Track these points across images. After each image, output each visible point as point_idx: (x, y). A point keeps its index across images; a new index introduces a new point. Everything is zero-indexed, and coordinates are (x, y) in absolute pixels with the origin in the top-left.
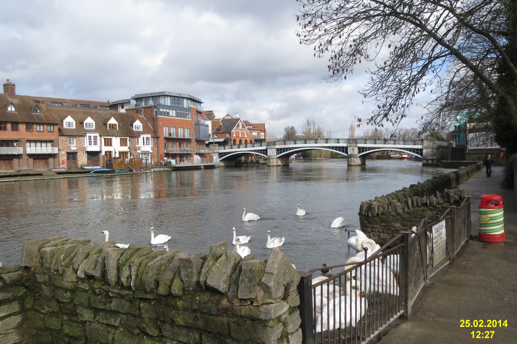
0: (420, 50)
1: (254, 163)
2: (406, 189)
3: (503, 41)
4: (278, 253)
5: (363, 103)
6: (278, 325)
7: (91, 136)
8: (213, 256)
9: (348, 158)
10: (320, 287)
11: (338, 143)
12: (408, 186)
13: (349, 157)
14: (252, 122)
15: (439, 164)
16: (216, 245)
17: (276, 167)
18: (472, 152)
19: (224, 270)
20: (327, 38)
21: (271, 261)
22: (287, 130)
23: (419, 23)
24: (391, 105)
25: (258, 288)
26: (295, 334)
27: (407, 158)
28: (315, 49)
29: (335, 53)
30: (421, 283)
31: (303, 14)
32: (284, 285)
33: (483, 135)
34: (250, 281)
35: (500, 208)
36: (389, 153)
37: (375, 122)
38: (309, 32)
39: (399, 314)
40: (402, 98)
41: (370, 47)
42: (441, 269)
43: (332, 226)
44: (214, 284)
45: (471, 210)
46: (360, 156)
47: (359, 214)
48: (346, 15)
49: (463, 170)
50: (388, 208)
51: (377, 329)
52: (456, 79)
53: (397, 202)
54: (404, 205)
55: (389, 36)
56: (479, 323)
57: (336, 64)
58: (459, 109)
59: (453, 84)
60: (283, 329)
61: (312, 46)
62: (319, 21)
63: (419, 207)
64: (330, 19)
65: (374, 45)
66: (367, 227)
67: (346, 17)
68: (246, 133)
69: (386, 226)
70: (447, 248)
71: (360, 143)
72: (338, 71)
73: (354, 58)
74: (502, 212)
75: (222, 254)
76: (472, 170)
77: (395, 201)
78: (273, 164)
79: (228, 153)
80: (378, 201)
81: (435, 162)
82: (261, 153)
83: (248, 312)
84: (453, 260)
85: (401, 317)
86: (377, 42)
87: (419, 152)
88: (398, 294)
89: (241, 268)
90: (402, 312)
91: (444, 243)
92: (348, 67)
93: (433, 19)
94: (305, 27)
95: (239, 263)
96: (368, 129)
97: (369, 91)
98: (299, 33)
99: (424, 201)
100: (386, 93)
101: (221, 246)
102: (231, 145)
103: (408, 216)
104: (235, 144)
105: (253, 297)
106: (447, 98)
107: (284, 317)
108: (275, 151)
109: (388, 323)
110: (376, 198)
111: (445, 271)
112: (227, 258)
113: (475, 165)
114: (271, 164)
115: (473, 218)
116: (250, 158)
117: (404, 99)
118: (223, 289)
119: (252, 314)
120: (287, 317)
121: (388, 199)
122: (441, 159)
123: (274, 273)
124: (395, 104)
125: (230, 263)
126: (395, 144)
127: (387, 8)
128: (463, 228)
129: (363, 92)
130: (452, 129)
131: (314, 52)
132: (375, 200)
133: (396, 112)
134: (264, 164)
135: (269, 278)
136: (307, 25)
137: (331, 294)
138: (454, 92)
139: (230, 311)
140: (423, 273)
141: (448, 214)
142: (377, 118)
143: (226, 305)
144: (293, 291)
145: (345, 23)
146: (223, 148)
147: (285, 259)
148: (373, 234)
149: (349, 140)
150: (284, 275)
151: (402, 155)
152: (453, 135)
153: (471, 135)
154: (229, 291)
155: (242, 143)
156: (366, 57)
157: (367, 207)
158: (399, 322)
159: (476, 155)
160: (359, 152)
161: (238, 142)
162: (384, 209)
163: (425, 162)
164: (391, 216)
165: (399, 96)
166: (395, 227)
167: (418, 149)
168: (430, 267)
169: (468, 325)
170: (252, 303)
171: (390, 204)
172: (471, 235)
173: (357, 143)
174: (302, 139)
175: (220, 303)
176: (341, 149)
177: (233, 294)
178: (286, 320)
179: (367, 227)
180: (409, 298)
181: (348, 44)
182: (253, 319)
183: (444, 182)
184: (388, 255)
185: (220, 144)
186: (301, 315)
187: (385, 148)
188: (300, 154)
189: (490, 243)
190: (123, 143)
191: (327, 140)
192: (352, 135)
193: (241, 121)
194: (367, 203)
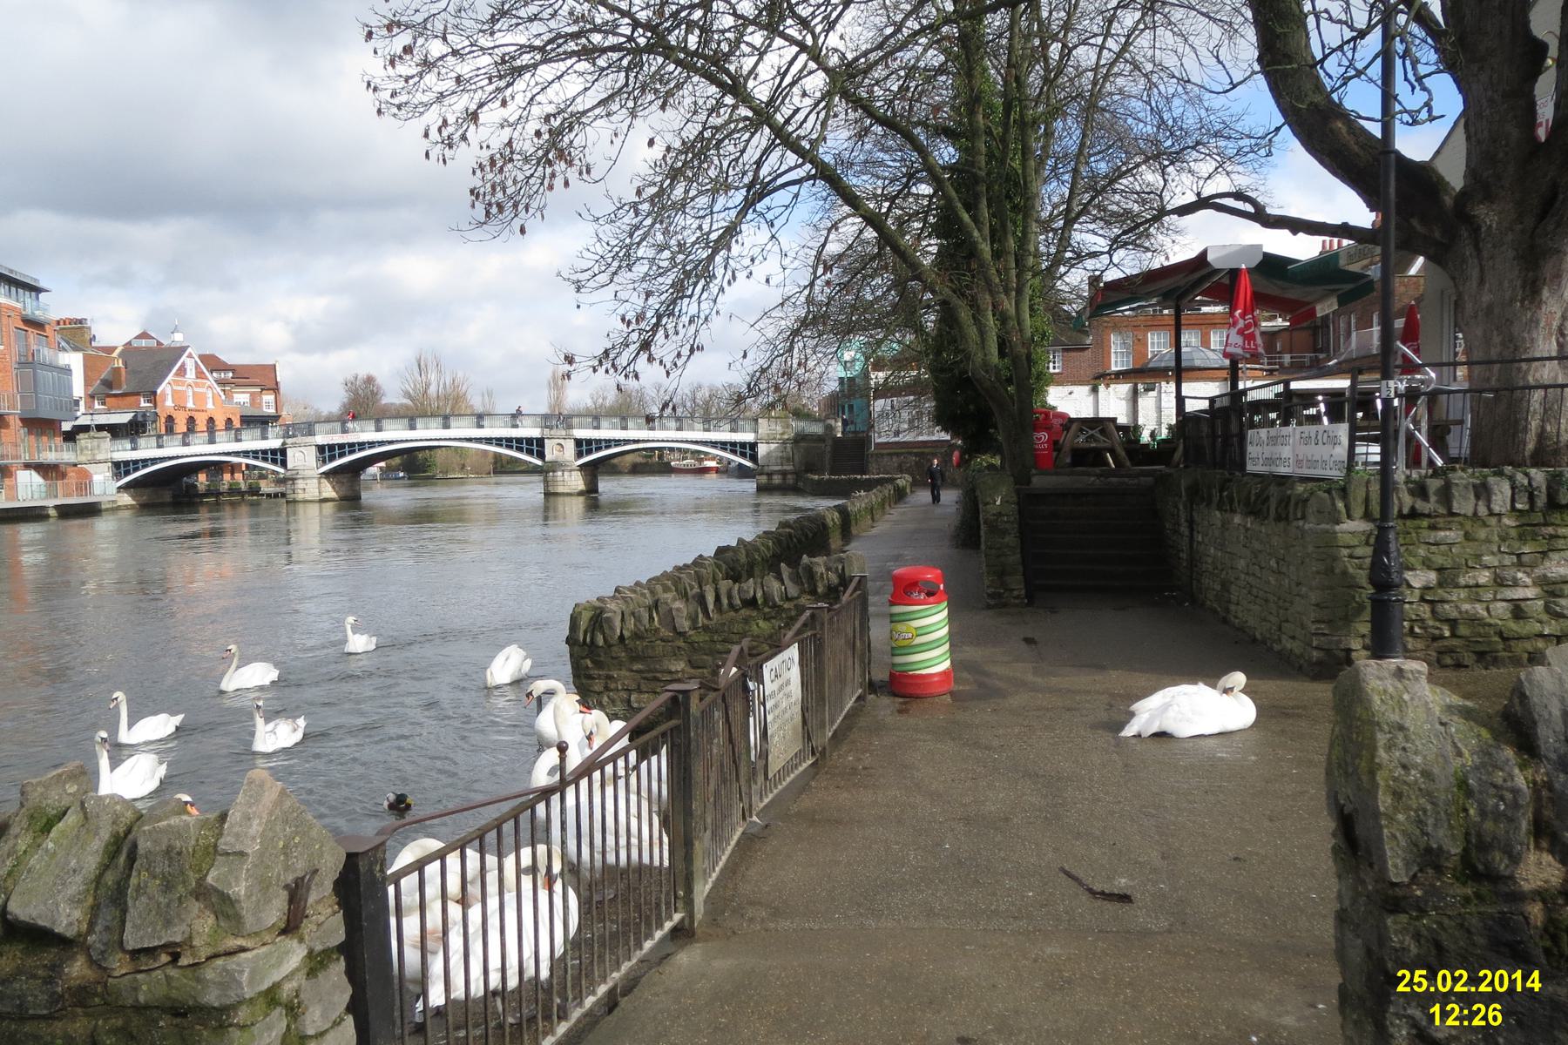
0: (737, 160)
1: (242, 494)
3: (946, 153)
4: (261, 786)
6: (267, 1015)
8: (32, 817)
9: (547, 472)
12: (710, 552)
15: (801, 484)
16: (43, 779)
17: (317, 505)
19: (73, 863)
20: (464, 102)
21: (238, 815)
22: (351, 386)
24: (659, 317)
25: (195, 906)
26: (329, 1037)
27: (717, 470)
28: (426, 135)
29: (491, 152)
30: (733, 829)
31: (386, 22)
32: (286, 887)
34: (168, 887)
35: (938, 602)
36: (667, 457)
37: (613, 365)
38: (406, 81)
39: (668, 925)
40: (690, 297)
41: (594, 139)
43: (273, 674)
44: (34, 914)
45: (871, 609)
46: (581, 466)
47: (567, 642)
48: (522, 40)
50: (651, 618)
52: (834, 248)
53: (674, 600)
54: (694, 606)
56: (1455, 980)
58: (845, 331)
60: (288, 1026)
61: (418, 125)
63: (737, 611)
64: (472, 45)
65: (607, 135)
66: (590, 677)
67: (522, 46)
68: (210, 395)
70: (804, 722)
72: (500, 207)
73: (549, 171)
74: (946, 612)
75: (68, 808)
76: (883, 500)
77: (669, 596)
79: (146, 462)
81: (790, 479)
82: (265, 460)
83: (161, 991)
84: (823, 753)
85: (675, 931)
87: (279, 457)
88: (666, 863)
89: (135, 846)
90: (677, 917)
91: (798, 708)
93: (766, 70)
94: (392, 63)
95: (129, 831)
96: (591, 387)
97: (590, 273)
98: (376, 81)
100: (643, 280)
101: (65, 783)
102: (159, 437)
104: (170, 430)
105: (178, 939)
106: (810, 301)
107: (288, 988)
108: (312, 453)
109: (638, 955)
110: (617, 590)
111: (801, 787)
112: (86, 818)
113: (890, 487)
114: (300, 496)
115: (878, 631)
116: (227, 477)
117: (695, 298)
118: (71, 924)
119: (174, 994)
120: (300, 987)
121: (652, 592)
124: (672, 314)
125: (96, 834)
126: (679, 429)
127: (641, 31)
128: (850, 662)
129: (571, 277)
130: (832, 386)
131: (425, 144)
134: (276, 495)
135: (231, 871)
138: (828, 283)
139: (96, 995)
140: (741, 799)
141: (805, 625)
142: (619, 354)
143: (84, 977)
144: (318, 902)
145: (518, 63)
146: (128, 446)
147: (288, 804)
149: (545, 417)
151: (701, 460)
152: (835, 404)
153: (879, 405)
156: (584, 169)
157: (591, 619)
158: (670, 948)
160: (579, 455)
161: (181, 426)
162: (640, 621)
163: (763, 479)
165: (679, 291)
166: (671, 672)
167: (743, 445)
168: (760, 779)
169: (1420, 984)
170: (175, 957)
171: (656, 605)
172: (870, 680)
173: (570, 427)
174: (402, 412)
176: (524, 446)
177: (105, 937)
178: (297, 996)
179: (590, 677)
180: (698, 876)
181: (532, 126)
182: (178, 1011)
183: (810, 535)
185: (115, 431)
186: (352, 974)
188: (397, 460)
189: (918, 697)
191: (480, 417)
192: (558, 402)
193: (190, 356)
194: (590, 607)
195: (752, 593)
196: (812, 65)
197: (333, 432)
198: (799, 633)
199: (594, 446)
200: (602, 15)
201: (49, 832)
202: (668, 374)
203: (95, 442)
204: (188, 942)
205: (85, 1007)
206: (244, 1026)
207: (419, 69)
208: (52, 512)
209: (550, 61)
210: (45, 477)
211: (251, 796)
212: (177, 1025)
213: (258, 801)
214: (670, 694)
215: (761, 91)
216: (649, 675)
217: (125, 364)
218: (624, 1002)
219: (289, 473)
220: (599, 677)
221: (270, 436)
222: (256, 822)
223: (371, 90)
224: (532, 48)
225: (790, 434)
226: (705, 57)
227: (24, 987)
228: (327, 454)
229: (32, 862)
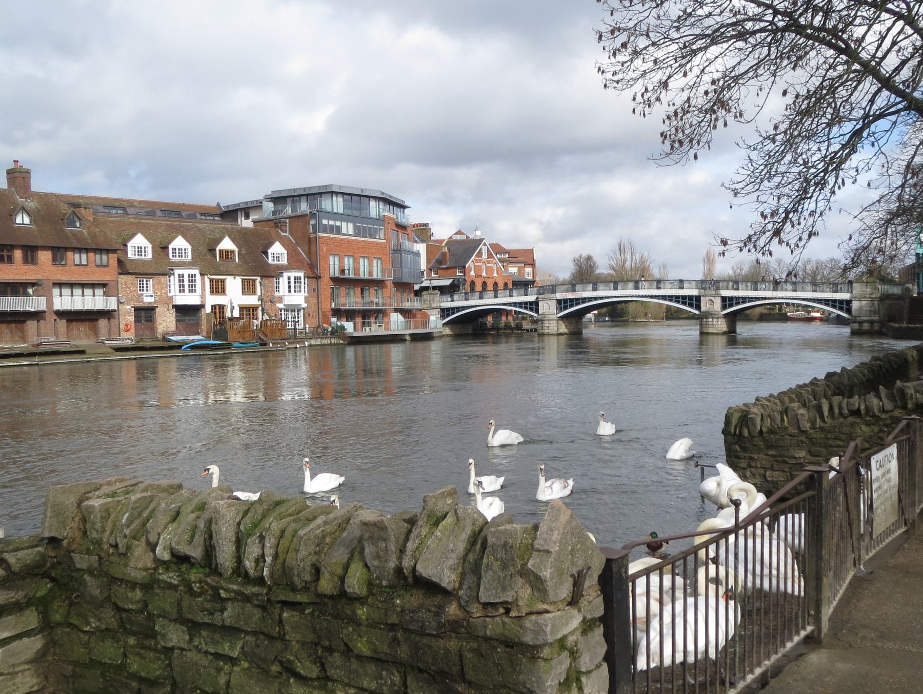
2: (819, 381)
4: (559, 510)
5: (731, 207)
6: (559, 655)
7: (183, 275)
8: (429, 516)
9: (702, 319)
11: (682, 288)
12: (821, 376)
15: (884, 330)
16: (435, 494)
17: (556, 337)
20: (660, 76)
21: (545, 527)
22: (577, 262)
23: (843, 46)
24: (787, 212)
25: (520, 581)
26: (594, 674)
27: (821, 319)
28: (634, 99)
29: (675, 107)
30: (847, 572)
31: (611, 28)
32: (572, 576)
34: (504, 567)
36: (785, 309)
37: (755, 246)
38: (622, 65)
39: (803, 634)
40: (811, 198)
42: (889, 544)
44: (430, 574)
47: (723, 433)
48: (697, 31)
50: (782, 420)
53: (799, 408)
54: (813, 412)
55: (783, 72)
57: (677, 130)
60: (571, 664)
61: (629, 93)
62: (642, 42)
63: (845, 418)
64: (665, 38)
65: (754, 90)
66: (738, 457)
67: (698, 35)
70: (900, 500)
72: (681, 143)
73: (714, 117)
75: (448, 513)
79: (459, 309)
83: (499, 630)
84: (913, 524)
85: (808, 639)
86: (759, 84)
87: (534, 306)
88: (802, 594)
89: (485, 540)
90: (809, 629)
91: (895, 491)
92: (701, 135)
93: (872, 38)
94: (614, 54)
95: (481, 530)
98: (604, 67)
99: (854, 405)
100: (777, 187)
101: (446, 497)
102: (466, 293)
103: (822, 436)
104: (472, 290)
105: (510, 600)
106: (900, 198)
107: (571, 640)
108: (553, 305)
109: (782, 652)
110: (757, 399)
111: (896, 547)
112: (458, 519)
114: (546, 331)
116: (504, 318)
117: (814, 199)
118: (450, 582)
119: (507, 633)
120: (578, 639)
122: (890, 321)
123: (552, 550)
124: (796, 211)
125: (464, 530)
126: (795, 290)
127: (780, 17)
129: (731, 187)
130: (911, 260)
132: (755, 404)
133: (798, 227)
134: (532, 330)
135: (541, 562)
136: (619, 50)
138: (915, 185)
140: (853, 551)
141: (902, 431)
142: (758, 239)
143: (456, 615)
144: (589, 587)
145: (694, 47)
146: (449, 299)
147: (574, 523)
148: (751, 472)
149: (702, 282)
150: (572, 555)
151: (809, 312)
154: (460, 587)
155: (488, 289)
156: (738, 114)
157: (740, 418)
158: (803, 650)
161: (479, 288)
162: (775, 422)
163: (856, 326)
165: (803, 194)
166: (795, 458)
167: (841, 302)
168: (867, 539)
170: (508, 611)
171: (786, 411)
173: (718, 289)
175: (444, 611)
177: (469, 593)
178: (576, 646)
179: (738, 457)
180: (824, 602)
181: (702, 89)
183: (896, 366)
185: (442, 290)
186: (607, 636)
187: (776, 298)
188: (604, 310)
190: (248, 288)
192: (710, 271)
193: (485, 244)
195: (857, 405)
196: (909, 30)
198: (895, 438)
199: (734, 301)
200: (752, 9)
201: (438, 526)
202: (792, 251)
203: (432, 297)
204: (515, 603)
205: (457, 633)
206: (546, 660)
207: (631, 57)
208: (408, 338)
209: (716, 44)
210: (404, 317)
211: (553, 516)
212: (507, 652)
213: (557, 519)
214: (808, 473)
215: (867, 52)
216: (780, 459)
217: (449, 250)
218: (773, 682)
219: (540, 317)
220: (744, 458)
221: (619, 287)
222: (556, 533)
223: (600, 72)
224: (704, 36)
225: (877, 295)
226: (827, 30)
227: (424, 616)
228: (563, 305)
229: (429, 543)
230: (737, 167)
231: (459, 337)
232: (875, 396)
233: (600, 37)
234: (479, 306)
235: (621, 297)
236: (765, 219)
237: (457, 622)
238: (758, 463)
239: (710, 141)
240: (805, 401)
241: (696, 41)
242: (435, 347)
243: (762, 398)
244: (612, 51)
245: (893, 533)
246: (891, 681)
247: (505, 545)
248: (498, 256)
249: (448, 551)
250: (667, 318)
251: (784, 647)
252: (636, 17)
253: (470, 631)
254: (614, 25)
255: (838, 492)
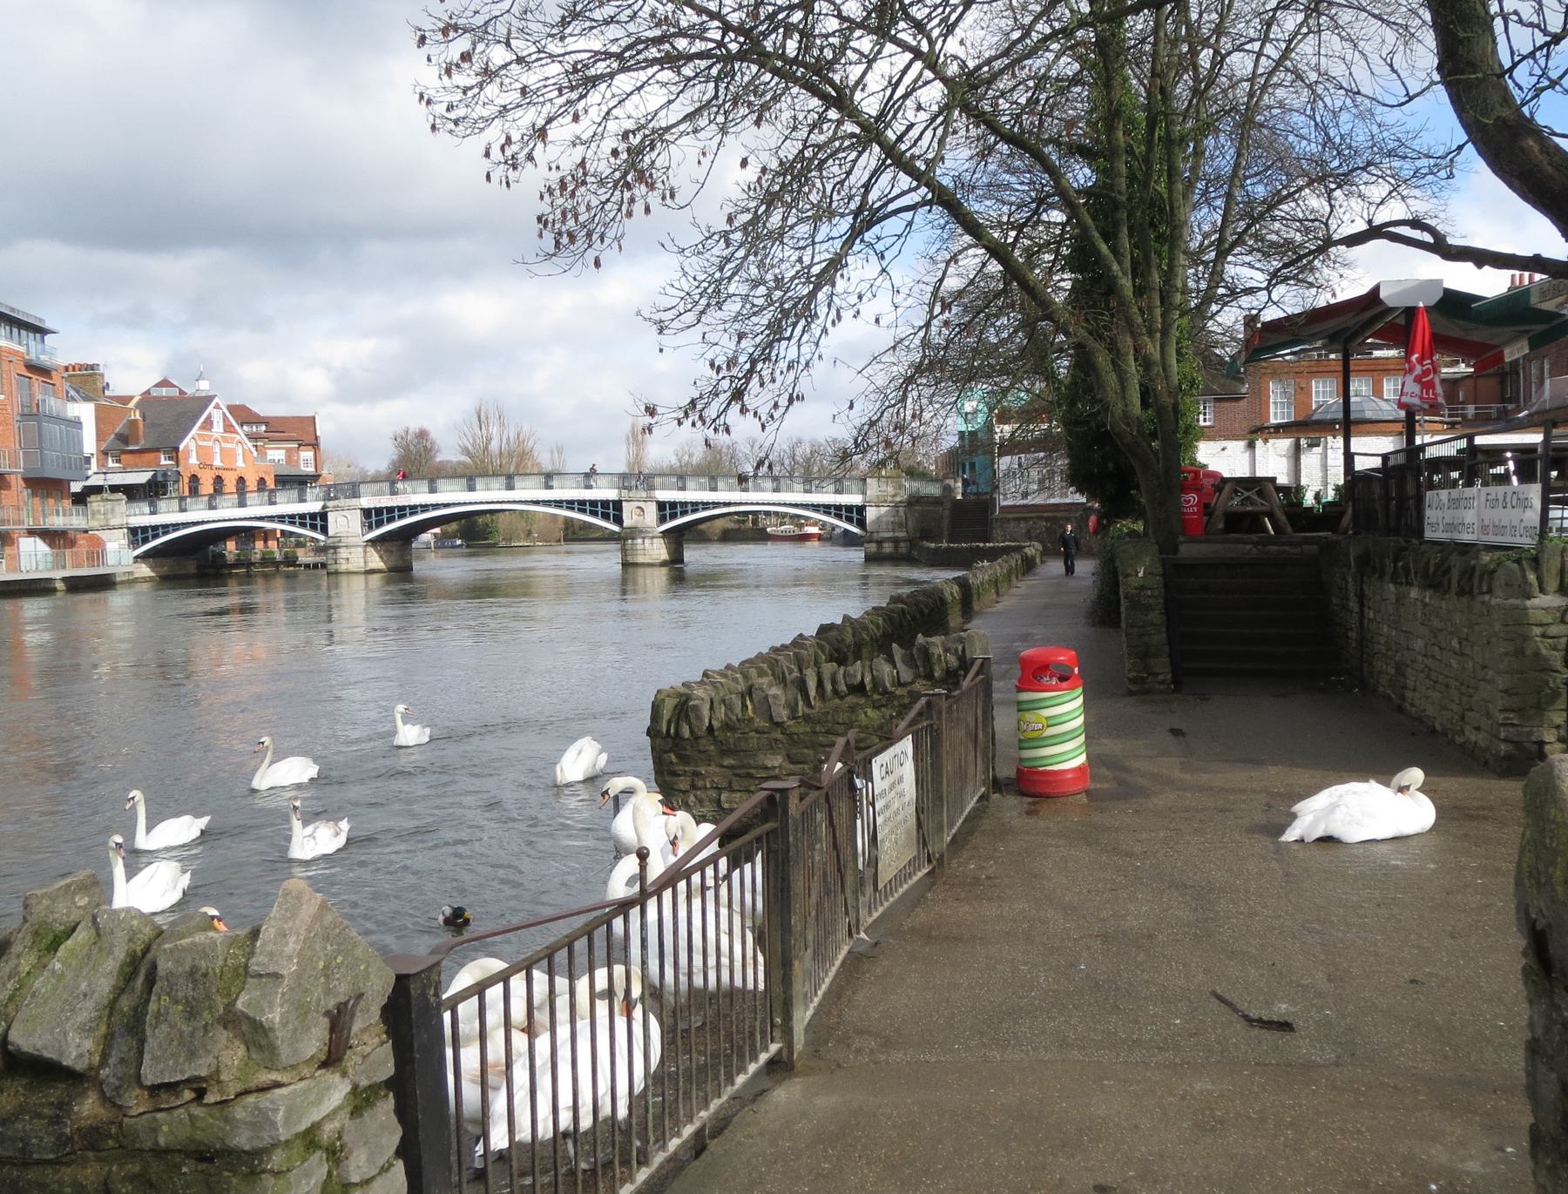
1: (276, 564)
2: (806, 639)
3: (1081, 175)
4: (299, 898)
5: (661, 350)
6: (305, 1160)
8: (36, 933)
9: (625, 539)
10: (500, 987)
12: (811, 631)
13: (624, 538)
14: (263, 409)
15: (915, 553)
16: (50, 890)
17: (363, 577)
18: (1011, 516)
19: (84, 986)
20: (530, 117)
21: (272, 931)
22: (401, 441)
23: (834, 94)
24: (754, 362)
25: (223, 1036)
27: (820, 538)
28: (487, 155)
29: (561, 174)
30: (838, 948)
31: (441, 25)
32: (327, 1013)
33: (1038, 461)
34: (192, 1013)
35: (1073, 688)
37: (701, 417)
38: (465, 93)
39: (763, 1057)
40: (789, 339)
42: (905, 894)
44: (39, 1044)
45: (995, 696)
47: (648, 733)
48: (597, 45)
49: (982, 573)
50: (744, 706)
51: (691, 1120)
53: (771, 685)
54: (793, 692)
55: (739, 127)
57: (564, 214)
58: (966, 378)
59: (943, 299)
60: (329, 1173)
61: (477, 143)
62: (499, 55)
63: (842, 698)
64: (539, 52)
65: (693, 154)
66: (675, 774)
67: (597, 53)
68: (240, 451)
69: (740, 767)
70: (919, 825)
71: (663, 488)
72: (572, 237)
73: (627, 195)
74: (1081, 700)
75: (78, 923)
76: (1010, 571)
77: (765, 681)
78: (352, 567)
79: (166, 528)
80: (713, 683)
81: (903, 548)
82: (303, 525)
83: (184, 1132)
84: (941, 860)
85: (772, 1064)
86: (701, 145)
87: (319, 522)
88: (761, 986)
90: (774, 1048)
92: (606, 225)
93: (875, 81)
94: (448, 72)
95: (147, 950)
97: (674, 312)
98: (431, 93)
99: (855, 676)
100: (735, 320)
101: (74, 894)
102: (182, 499)
103: (808, 729)
104: (194, 491)
106: (925, 343)
107: (329, 1128)
108: (356, 518)
109: (729, 1091)
110: (705, 674)
111: (916, 899)
112: (98, 935)
113: (1018, 556)
114: (343, 567)
115: (1003, 722)
116: (259, 545)
118: (81, 1056)
119: (199, 1135)
120: (343, 1127)
121: (746, 677)
122: (922, 538)
123: (285, 972)
124: (768, 359)
125: (110, 952)
126: (776, 490)
127: (732, 35)
128: (971, 757)
130: (951, 441)
131: (486, 165)
132: (701, 683)
133: (771, 386)
134: (315, 566)
135: (263, 995)
136: (458, 66)
137: (540, 1008)
139: (109, 1136)
140: (847, 913)
141: (920, 714)
142: (708, 404)
143: (95, 1117)
144: (363, 1031)
145: (592, 72)
146: (147, 510)
147: (329, 918)
148: (696, 797)
149: (623, 476)
150: (327, 976)
151: (801, 527)
152: (955, 461)
153: (1004, 463)
154: (104, 1062)
155: (226, 490)
157: (676, 707)
158: (765, 1083)
159: (1023, 525)
160: (662, 520)
161: (207, 487)
162: (732, 711)
163: (873, 547)
164: (753, 734)
165: (776, 331)
166: (767, 768)
167: (849, 508)
168: (869, 889)
170: (200, 1094)
173: (651, 488)
175: (69, 1113)
177: (120, 1071)
178: (339, 1138)
179: (675, 774)
181: (609, 144)
182: (204, 1155)
184: (746, 862)
185: (132, 493)
186: (402, 1112)
187: (746, 504)
188: (454, 526)
189: (1048, 797)
191: (549, 476)
192: (638, 459)
193: (217, 407)
195: (859, 678)
197: (380, 493)
199: (679, 509)
201: (56, 950)
202: (763, 427)
203: (109, 505)
204: (215, 1077)
205: (98, 1151)
206: (279, 1173)
207: (479, 79)
208: (60, 586)
210: (51, 545)
211: (286, 910)
212: (202, 1171)
213: (294, 916)
214: (766, 793)
216: (743, 771)
218: (713, 1145)
219: (331, 540)
221: (478, 487)
223: (424, 103)
224: (608, 55)
225: (903, 496)
228: (374, 518)
230: (664, 284)
231: (167, 580)
232: (886, 660)
233: (422, 40)
234: (208, 522)
235: (481, 503)
236: (718, 373)
237: (98, 1128)
238: (708, 780)
239: (622, 236)
240: (783, 673)
241: (595, 62)
242: (118, 600)
243: (713, 671)
244: (444, 65)
245: (910, 877)
246: (895, 1113)
247: (192, 973)
248: (245, 428)
249: (78, 997)
250: (567, 539)
251: (733, 1084)
252: (487, 8)
253: (125, 1141)
254: (447, 19)
255: (818, 819)
